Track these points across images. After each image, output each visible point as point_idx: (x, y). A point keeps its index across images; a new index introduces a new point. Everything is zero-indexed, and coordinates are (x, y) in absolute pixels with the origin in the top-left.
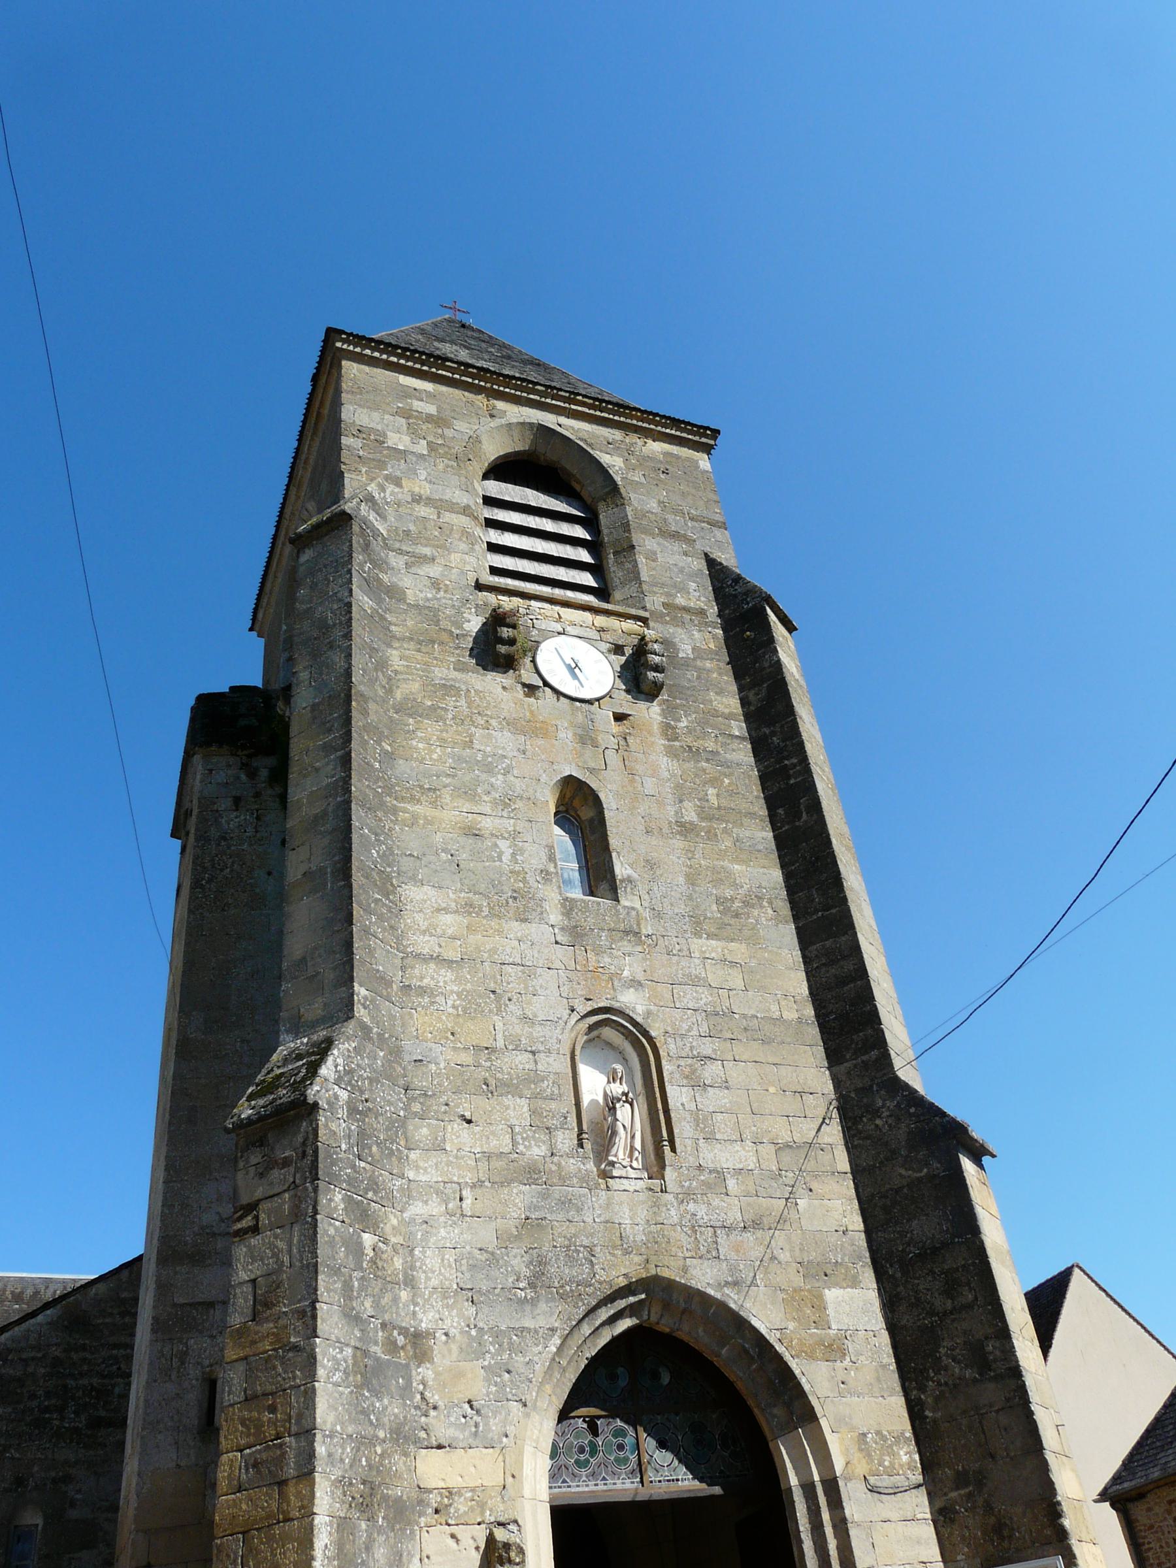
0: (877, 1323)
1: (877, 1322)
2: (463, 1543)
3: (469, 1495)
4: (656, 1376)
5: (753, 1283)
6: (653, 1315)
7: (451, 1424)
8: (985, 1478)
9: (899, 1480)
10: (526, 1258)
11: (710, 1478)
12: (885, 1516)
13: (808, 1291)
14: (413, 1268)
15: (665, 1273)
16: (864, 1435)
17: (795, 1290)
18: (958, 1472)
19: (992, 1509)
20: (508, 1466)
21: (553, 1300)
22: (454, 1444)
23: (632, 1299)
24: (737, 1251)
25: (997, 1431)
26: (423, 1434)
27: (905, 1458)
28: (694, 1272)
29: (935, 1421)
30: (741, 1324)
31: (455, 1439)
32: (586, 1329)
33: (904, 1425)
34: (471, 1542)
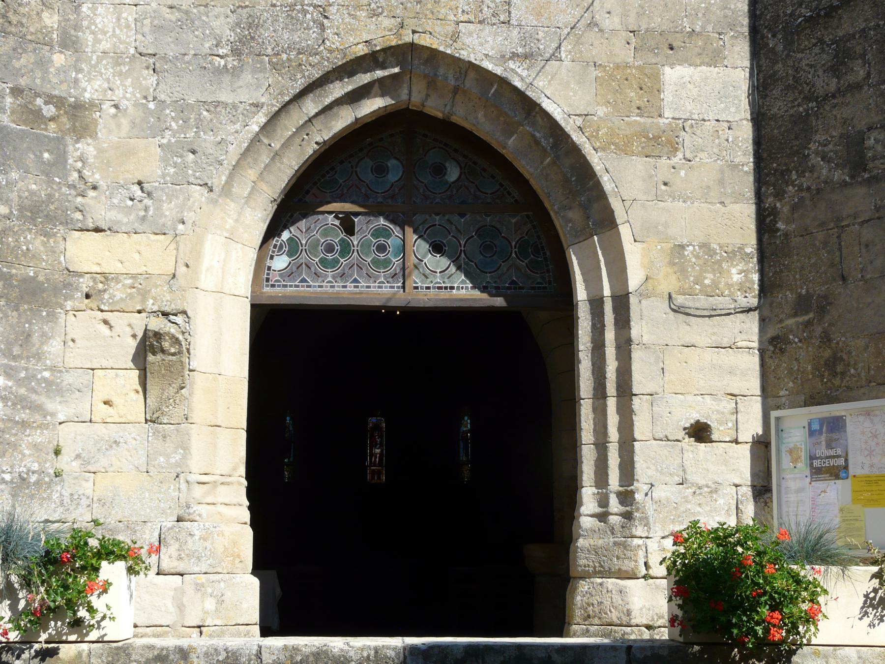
0: (738, 111)
1: (739, 110)
2: (117, 329)
3: (129, 282)
4: (440, 170)
5: (555, 56)
6: (416, 95)
7: (113, 206)
8: (830, 304)
9: (723, 302)
10: (233, 19)
11: (497, 288)
12: (688, 340)
13: (639, 68)
14: (77, 27)
15: (425, 41)
16: (682, 247)
17: (617, 67)
18: (800, 296)
19: (829, 340)
20: (181, 255)
21: (263, 70)
22: (115, 228)
23: (379, 74)
24: (539, 14)
25: (856, 248)
26: (78, 216)
27: (736, 278)
28: (468, 41)
29: (786, 235)
30: (529, 107)
31: (118, 222)
32: (311, 106)
33: (747, 236)
34: (128, 329)
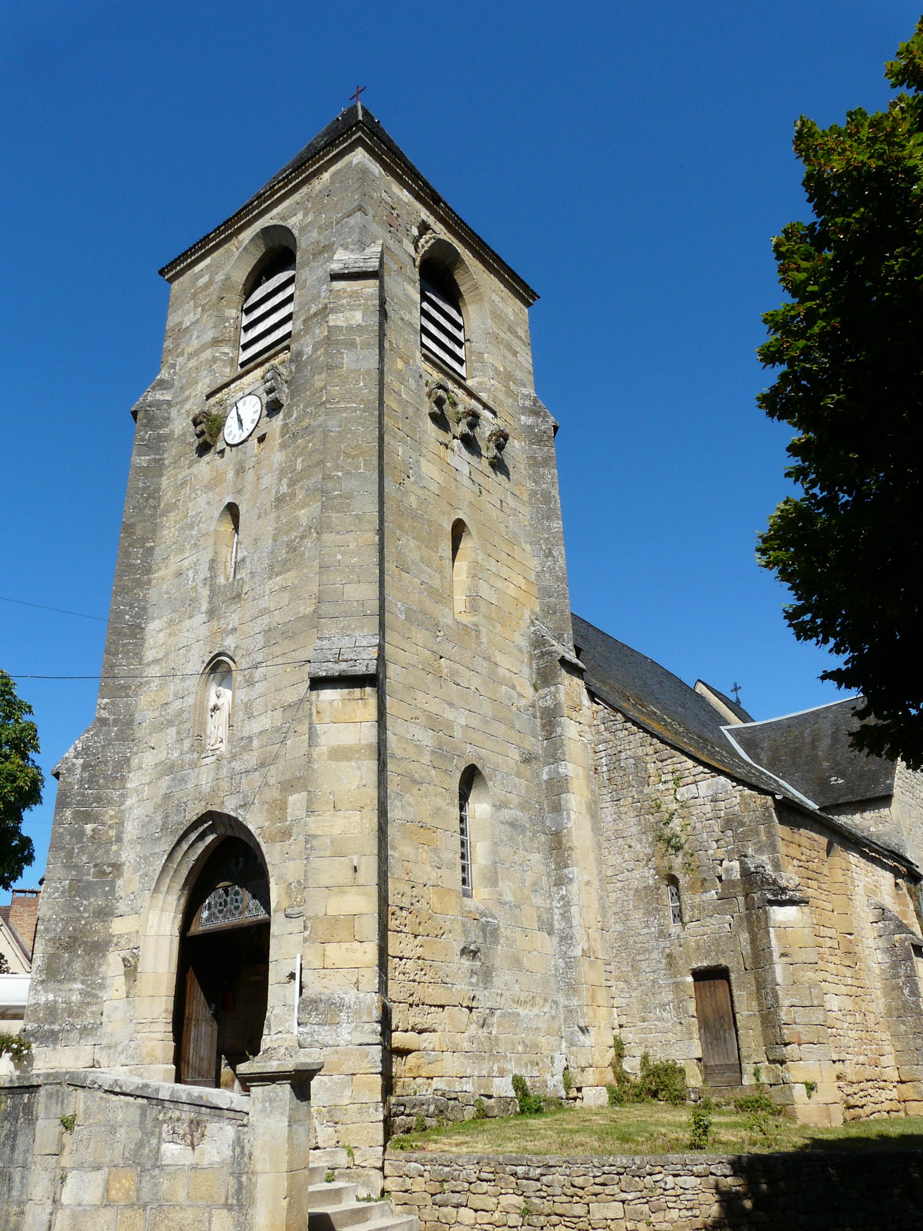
23: (206, 825)
